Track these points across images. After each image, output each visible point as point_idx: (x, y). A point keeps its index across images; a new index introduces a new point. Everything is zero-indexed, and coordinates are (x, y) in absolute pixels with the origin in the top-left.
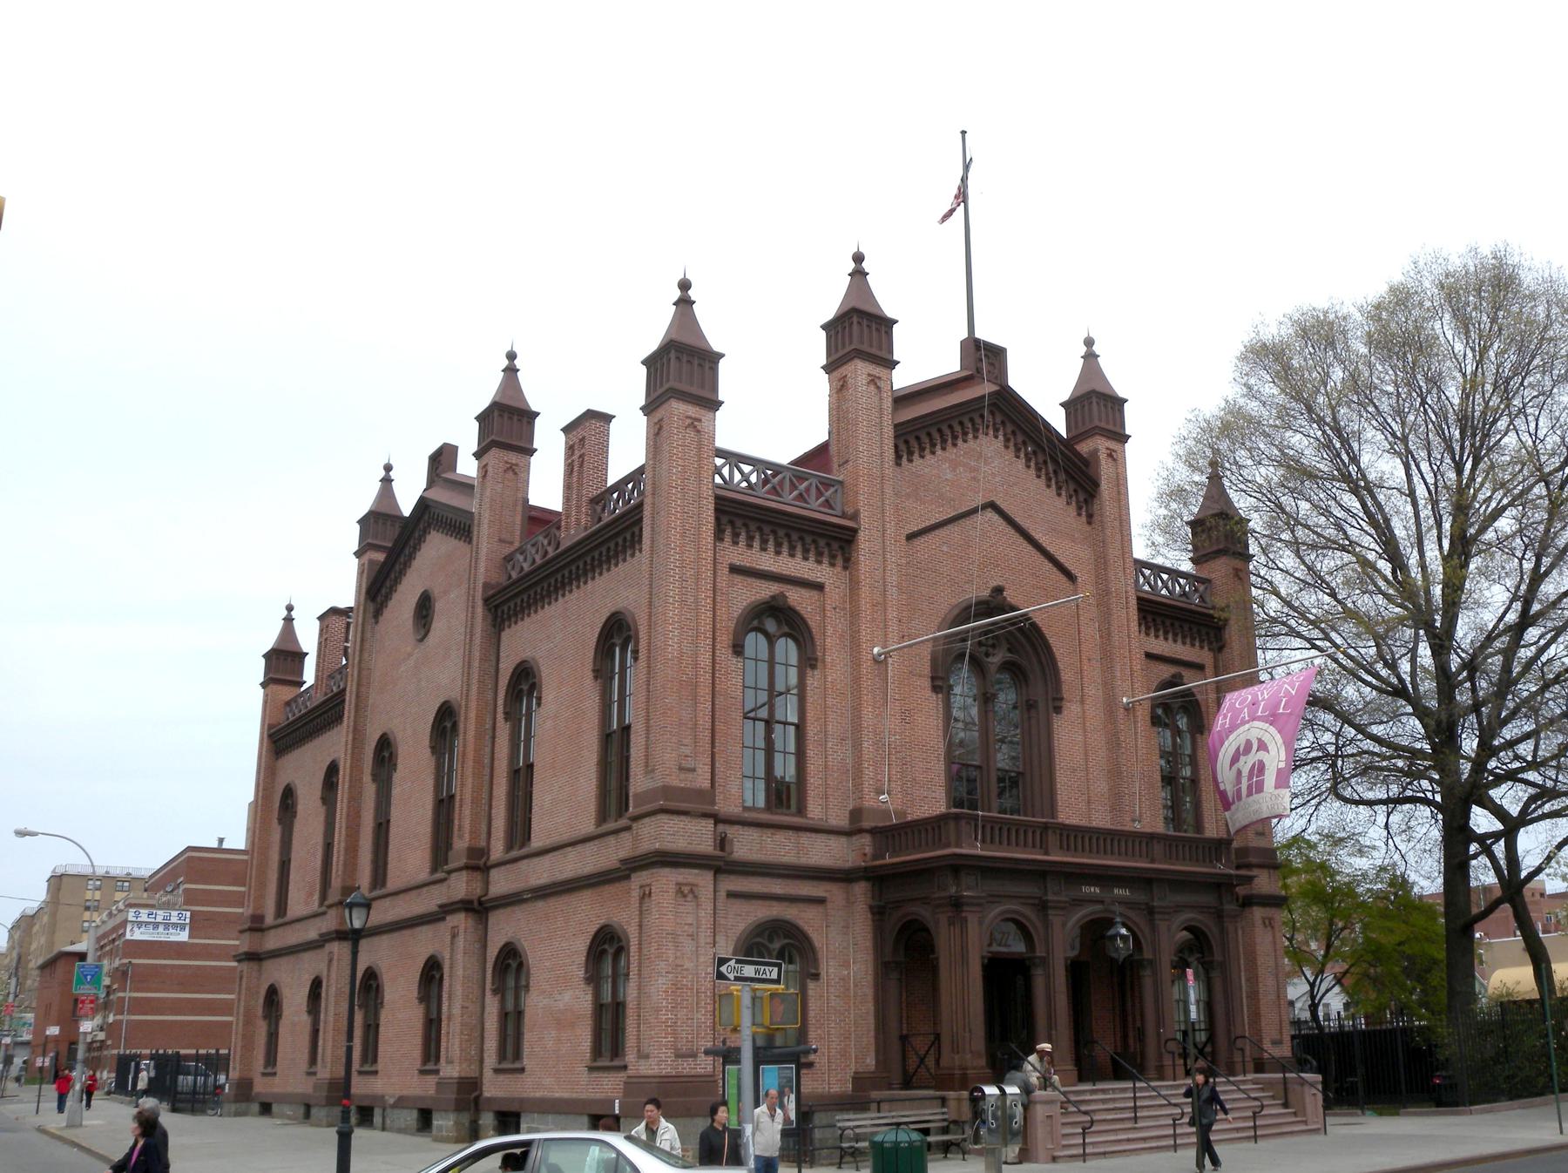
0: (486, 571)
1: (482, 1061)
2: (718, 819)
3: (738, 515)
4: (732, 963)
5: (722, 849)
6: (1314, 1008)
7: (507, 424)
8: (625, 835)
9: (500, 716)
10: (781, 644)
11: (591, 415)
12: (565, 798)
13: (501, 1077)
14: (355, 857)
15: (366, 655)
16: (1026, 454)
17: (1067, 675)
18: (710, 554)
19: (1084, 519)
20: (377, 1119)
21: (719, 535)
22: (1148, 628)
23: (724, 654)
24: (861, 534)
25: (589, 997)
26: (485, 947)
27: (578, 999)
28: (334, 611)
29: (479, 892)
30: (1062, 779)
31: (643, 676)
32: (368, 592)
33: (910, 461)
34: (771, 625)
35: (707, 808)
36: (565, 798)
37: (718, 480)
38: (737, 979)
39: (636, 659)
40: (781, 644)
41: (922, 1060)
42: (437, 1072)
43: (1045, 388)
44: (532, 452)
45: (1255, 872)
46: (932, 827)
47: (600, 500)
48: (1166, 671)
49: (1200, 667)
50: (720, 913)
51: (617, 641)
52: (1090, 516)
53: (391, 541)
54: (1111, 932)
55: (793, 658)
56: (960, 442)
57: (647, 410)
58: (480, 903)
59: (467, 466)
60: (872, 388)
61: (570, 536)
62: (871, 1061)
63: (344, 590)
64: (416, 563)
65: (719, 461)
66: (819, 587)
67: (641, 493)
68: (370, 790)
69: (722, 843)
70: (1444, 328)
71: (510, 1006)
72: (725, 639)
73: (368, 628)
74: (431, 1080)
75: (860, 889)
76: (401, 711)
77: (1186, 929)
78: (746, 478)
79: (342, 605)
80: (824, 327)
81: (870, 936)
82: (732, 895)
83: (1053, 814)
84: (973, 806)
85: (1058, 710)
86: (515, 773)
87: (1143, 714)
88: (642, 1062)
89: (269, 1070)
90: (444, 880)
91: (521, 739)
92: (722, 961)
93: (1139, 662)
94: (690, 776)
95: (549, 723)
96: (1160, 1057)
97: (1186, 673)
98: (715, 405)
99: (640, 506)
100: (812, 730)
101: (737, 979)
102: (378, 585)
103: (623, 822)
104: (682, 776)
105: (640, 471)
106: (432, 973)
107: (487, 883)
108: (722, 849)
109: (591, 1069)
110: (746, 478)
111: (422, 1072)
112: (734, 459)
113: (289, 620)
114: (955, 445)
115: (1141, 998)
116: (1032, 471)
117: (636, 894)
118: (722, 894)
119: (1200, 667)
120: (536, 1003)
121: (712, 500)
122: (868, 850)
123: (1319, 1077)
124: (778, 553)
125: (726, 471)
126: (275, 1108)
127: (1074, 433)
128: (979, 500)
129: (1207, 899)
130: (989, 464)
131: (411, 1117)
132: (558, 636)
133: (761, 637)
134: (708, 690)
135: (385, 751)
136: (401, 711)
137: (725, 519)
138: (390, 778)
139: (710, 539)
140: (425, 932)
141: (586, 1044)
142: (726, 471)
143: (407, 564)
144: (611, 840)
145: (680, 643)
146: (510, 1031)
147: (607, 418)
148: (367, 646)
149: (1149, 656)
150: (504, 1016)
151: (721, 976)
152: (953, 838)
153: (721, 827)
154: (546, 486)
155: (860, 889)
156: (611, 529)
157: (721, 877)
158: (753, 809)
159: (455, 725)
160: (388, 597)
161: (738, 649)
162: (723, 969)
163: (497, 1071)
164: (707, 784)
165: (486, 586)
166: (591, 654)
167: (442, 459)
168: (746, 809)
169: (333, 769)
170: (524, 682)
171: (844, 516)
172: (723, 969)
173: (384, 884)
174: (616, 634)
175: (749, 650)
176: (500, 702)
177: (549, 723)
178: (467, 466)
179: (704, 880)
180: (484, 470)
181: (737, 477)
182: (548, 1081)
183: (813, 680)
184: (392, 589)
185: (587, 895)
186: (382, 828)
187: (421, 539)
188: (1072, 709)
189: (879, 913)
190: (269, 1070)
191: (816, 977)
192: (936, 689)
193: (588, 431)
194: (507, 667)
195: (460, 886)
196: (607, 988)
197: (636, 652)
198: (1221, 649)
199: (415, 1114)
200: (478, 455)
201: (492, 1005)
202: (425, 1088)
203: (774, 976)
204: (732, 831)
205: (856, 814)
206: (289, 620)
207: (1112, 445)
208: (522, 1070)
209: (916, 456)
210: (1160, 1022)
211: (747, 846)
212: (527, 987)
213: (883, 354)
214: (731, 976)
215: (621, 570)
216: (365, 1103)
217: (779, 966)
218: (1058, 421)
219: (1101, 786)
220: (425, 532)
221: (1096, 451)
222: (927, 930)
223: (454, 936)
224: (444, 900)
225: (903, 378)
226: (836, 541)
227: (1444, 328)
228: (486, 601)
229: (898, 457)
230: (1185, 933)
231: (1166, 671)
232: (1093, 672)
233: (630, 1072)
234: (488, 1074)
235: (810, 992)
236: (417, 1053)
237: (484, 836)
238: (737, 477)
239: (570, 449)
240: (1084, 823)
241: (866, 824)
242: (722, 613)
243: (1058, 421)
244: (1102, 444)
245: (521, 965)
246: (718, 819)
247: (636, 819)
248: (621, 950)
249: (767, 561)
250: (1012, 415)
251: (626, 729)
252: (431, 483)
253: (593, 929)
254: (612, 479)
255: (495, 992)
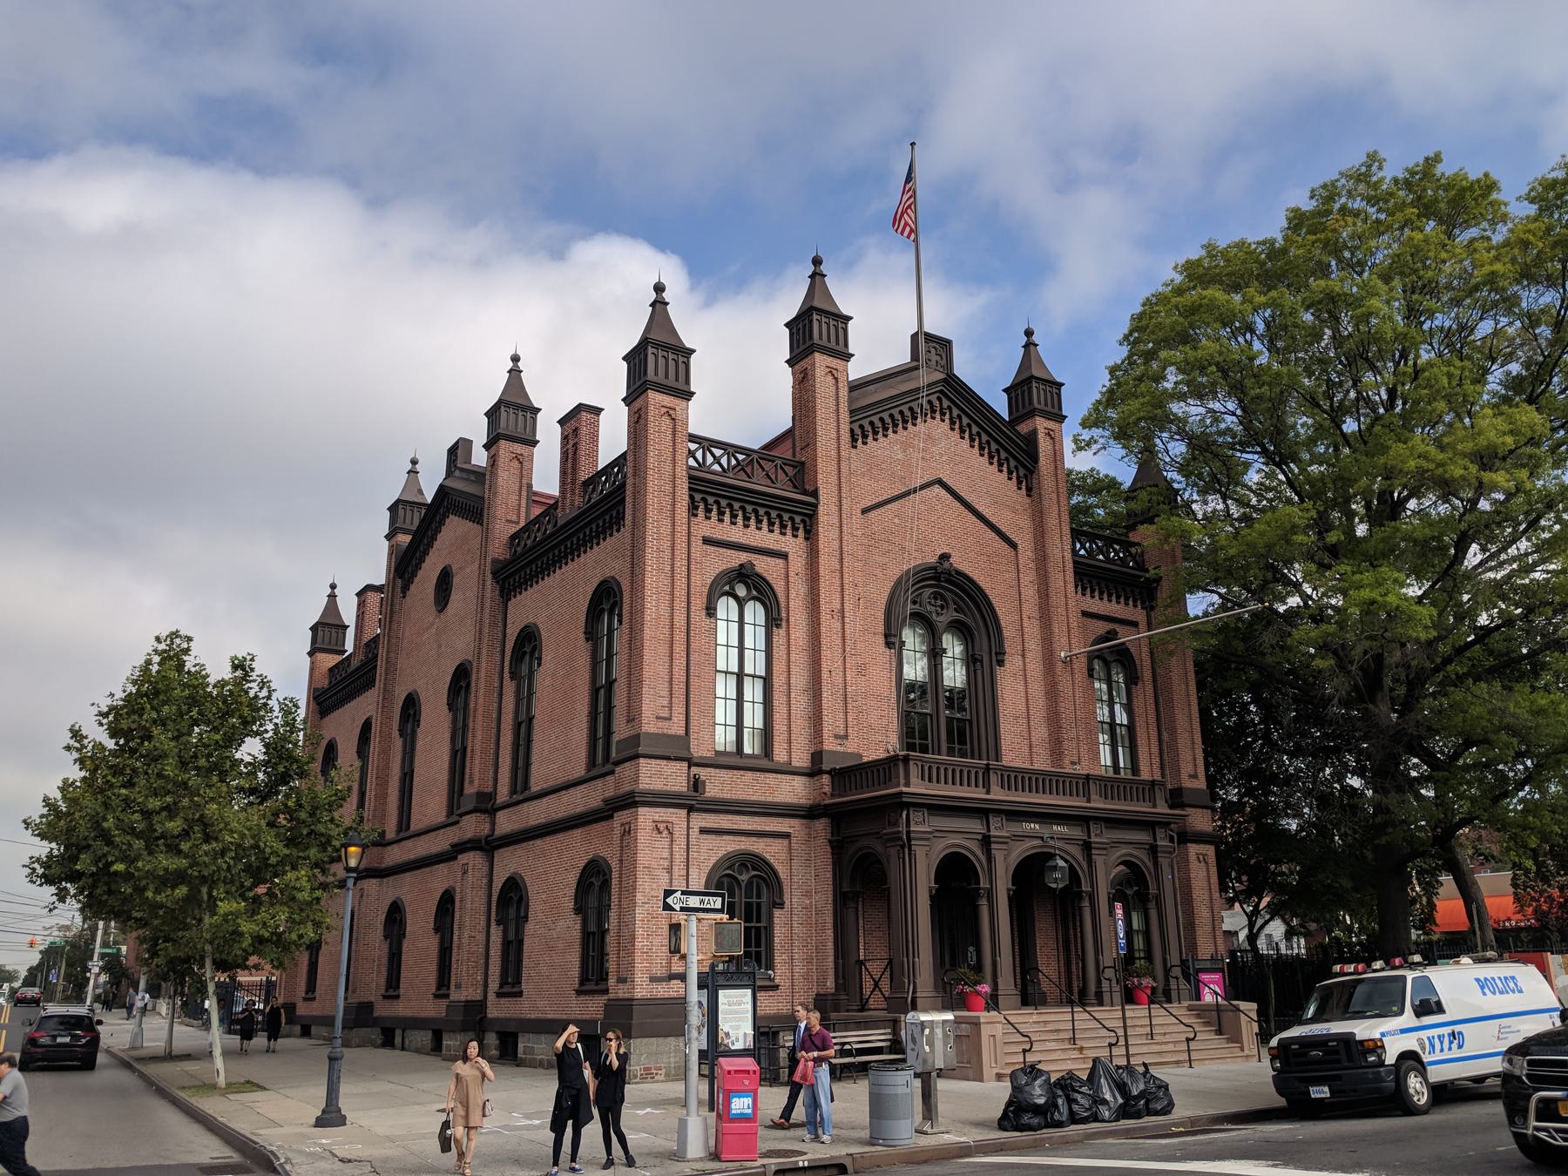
0: (498, 549)
1: (486, 985)
2: (691, 763)
3: (707, 492)
4: (678, 894)
5: (696, 790)
6: (1252, 938)
7: (511, 415)
8: (610, 778)
9: (507, 675)
10: (750, 607)
11: (580, 408)
12: (560, 747)
13: (503, 1000)
14: (385, 803)
15: (395, 627)
16: (971, 435)
17: (1009, 632)
18: (685, 527)
19: (1024, 491)
20: (398, 1040)
21: (693, 509)
22: (1084, 589)
23: (698, 614)
24: (820, 508)
25: (578, 927)
26: (491, 881)
27: (569, 927)
28: (369, 588)
29: (486, 832)
30: (1005, 727)
31: (626, 638)
32: (396, 570)
33: (865, 443)
34: (741, 591)
35: (684, 754)
36: (560, 747)
37: (692, 462)
38: (682, 909)
39: (620, 622)
40: (750, 607)
41: (876, 985)
42: (447, 996)
43: (987, 373)
44: (534, 443)
45: (1189, 811)
46: (886, 768)
47: (592, 481)
48: (1102, 627)
49: (1135, 624)
50: (693, 848)
51: (606, 606)
52: (1029, 490)
53: (419, 527)
54: (1051, 863)
55: (761, 619)
56: (909, 425)
57: (628, 401)
58: (488, 843)
59: (480, 458)
60: (830, 378)
61: (563, 516)
62: (831, 983)
63: (377, 571)
64: (437, 544)
65: (693, 446)
66: (784, 556)
67: (625, 476)
68: (398, 743)
69: (697, 784)
70: (1274, 1042)
71: (511, 936)
72: (699, 603)
73: (397, 601)
74: (444, 1003)
75: (821, 825)
76: (424, 674)
77: (1122, 863)
78: (717, 460)
79: (377, 583)
80: (787, 325)
81: (830, 868)
82: (703, 831)
83: (998, 757)
84: (924, 749)
85: (1001, 663)
86: (517, 726)
87: (1080, 665)
88: (621, 986)
89: (391, 992)
90: (457, 822)
91: (525, 699)
92: (668, 893)
93: (1075, 620)
94: (667, 723)
95: (548, 681)
96: (1099, 983)
97: (1119, 628)
98: (688, 395)
99: (623, 485)
100: (778, 681)
101: (682, 909)
102: (405, 565)
103: (609, 767)
104: (660, 724)
105: (624, 454)
106: (446, 904)
107: (493, 824)
108: (696, 790)
109: (579, 993)
110: (717, 460)
111: (436, 996)
112: (707, 444)
113: (332, 596)
114: (905, 428)
115: (1081, 926)
116: (976, 450)
117: (617, 832)
118: (694, 832)
119: (1135, 624)
120: (533, 932)
121: (686, 480)
122: (827, 789)
123: (1254, 1006)
124: (746, 526)
125: (699, 455)
126: (314, 1030)
127: (1016, 415)
128: (928, 478)
129: (1143, 837)
130: (937, 445)
131: (425, 1038)
132: (553, 606)
133: (732, 602)
134: (684, 647)
135: (411, 706)
136: (424, 674)
137: (698, 497)
138: (414, 733)
139: (685, 515)
140: (441, 869)
141: (575, 972)
142: (699, 455)
143: (430, 545)
144: (599, 783)
145: (657, 606)
146: (512, 957)
147: (597, 411)
148: (396, 617)
149: (1085, 614)
150: (506, 944)
151: (667, 907)
152: (902, 781)
153: (694, 770)
154: (546, 476)
155: (821, 825)
156: (601, 506)
157: (694, 815)
158: (724, 753)
159: (468, 685)
160: (414, 574)
161: (711, 611)
162: (669, 900)
163: (499, 995)
164: (682, 732)
165: (494, 561)
166: (583, 619)
167: (458, 451)
168: (717, 752)
169: (367, 727)
170: (528, 643)
171: (805, 493)
172: (669, 900)
173: (408, 828)
174: (607, 602)
175: (721, 613)
176: (507, 663)
177: (548, 681)
178: (480, 458)
179: (677, 816)
180: (493, 460)
181: (710, 459)
182: (541, 1003)
183: (779, 636)
184: (418, 567)
185: (578, 833)
186: (407, 777)
187: (442, 523)
188: (1013, 662)
189: (838, 847)
190: (391, 992)
191: (781, 905)
192: (889, 645)
193: (578, 421)
194: (513, 632)
195: (472, 826)
196: (592, 918)
197: (620, 615)
198: (1152, 608)
199: (430, 1033)
200: (487, 447)
201: (496, 934)
202: (435, 1010)
203: (718, 905)
204: (703, 773)
205: (817, 757)
206: (332, 596)
207: (1051, 425)
208: (520, 994)
209: (870, 439)
210: (1098, 950)
211: (718, 785)
212: (526, 917)
213: (841, 348)
214: (677, 907)
215: (608, 544)
216: (388, 1025)
217: (722, 896)
218: (1000, 405)
219: (1041, 733)
220: (445, 516)
221: (1034, 432)
222: (879, 862)
223: (465, 872)
224: (456, 840)
225: (857, 369)
226: (800, 514)
227: (1274, 1042)
228: (495, 574)
229: (854, 440)
230: (1122, 867)
231: (1102, 627)
232: (1032, 629)
233: (611, 996)
234: (491, 997)
235: (776, 921)
236: (432, 979)
237: (491, 783)
238: (710, 459)
239: (565, 438)
240: (1027, 766)
241: (825, 767)
242: (696, 579)
243: (1000, 405)
244: (1041, 424)
245: (521, 899)
246: (691, 763)
247: (617, 763)
248: (606, 884)
249: (736, 533)
250: (956, 400)
251: (610, 683)
252: (449, 474)
253: (582, 864)
254: (603, 460)
255: (499, 923)
